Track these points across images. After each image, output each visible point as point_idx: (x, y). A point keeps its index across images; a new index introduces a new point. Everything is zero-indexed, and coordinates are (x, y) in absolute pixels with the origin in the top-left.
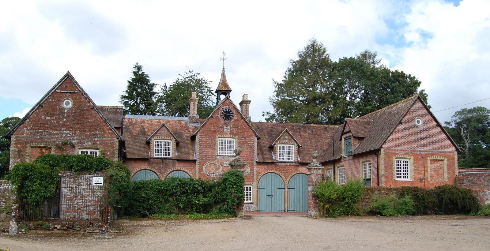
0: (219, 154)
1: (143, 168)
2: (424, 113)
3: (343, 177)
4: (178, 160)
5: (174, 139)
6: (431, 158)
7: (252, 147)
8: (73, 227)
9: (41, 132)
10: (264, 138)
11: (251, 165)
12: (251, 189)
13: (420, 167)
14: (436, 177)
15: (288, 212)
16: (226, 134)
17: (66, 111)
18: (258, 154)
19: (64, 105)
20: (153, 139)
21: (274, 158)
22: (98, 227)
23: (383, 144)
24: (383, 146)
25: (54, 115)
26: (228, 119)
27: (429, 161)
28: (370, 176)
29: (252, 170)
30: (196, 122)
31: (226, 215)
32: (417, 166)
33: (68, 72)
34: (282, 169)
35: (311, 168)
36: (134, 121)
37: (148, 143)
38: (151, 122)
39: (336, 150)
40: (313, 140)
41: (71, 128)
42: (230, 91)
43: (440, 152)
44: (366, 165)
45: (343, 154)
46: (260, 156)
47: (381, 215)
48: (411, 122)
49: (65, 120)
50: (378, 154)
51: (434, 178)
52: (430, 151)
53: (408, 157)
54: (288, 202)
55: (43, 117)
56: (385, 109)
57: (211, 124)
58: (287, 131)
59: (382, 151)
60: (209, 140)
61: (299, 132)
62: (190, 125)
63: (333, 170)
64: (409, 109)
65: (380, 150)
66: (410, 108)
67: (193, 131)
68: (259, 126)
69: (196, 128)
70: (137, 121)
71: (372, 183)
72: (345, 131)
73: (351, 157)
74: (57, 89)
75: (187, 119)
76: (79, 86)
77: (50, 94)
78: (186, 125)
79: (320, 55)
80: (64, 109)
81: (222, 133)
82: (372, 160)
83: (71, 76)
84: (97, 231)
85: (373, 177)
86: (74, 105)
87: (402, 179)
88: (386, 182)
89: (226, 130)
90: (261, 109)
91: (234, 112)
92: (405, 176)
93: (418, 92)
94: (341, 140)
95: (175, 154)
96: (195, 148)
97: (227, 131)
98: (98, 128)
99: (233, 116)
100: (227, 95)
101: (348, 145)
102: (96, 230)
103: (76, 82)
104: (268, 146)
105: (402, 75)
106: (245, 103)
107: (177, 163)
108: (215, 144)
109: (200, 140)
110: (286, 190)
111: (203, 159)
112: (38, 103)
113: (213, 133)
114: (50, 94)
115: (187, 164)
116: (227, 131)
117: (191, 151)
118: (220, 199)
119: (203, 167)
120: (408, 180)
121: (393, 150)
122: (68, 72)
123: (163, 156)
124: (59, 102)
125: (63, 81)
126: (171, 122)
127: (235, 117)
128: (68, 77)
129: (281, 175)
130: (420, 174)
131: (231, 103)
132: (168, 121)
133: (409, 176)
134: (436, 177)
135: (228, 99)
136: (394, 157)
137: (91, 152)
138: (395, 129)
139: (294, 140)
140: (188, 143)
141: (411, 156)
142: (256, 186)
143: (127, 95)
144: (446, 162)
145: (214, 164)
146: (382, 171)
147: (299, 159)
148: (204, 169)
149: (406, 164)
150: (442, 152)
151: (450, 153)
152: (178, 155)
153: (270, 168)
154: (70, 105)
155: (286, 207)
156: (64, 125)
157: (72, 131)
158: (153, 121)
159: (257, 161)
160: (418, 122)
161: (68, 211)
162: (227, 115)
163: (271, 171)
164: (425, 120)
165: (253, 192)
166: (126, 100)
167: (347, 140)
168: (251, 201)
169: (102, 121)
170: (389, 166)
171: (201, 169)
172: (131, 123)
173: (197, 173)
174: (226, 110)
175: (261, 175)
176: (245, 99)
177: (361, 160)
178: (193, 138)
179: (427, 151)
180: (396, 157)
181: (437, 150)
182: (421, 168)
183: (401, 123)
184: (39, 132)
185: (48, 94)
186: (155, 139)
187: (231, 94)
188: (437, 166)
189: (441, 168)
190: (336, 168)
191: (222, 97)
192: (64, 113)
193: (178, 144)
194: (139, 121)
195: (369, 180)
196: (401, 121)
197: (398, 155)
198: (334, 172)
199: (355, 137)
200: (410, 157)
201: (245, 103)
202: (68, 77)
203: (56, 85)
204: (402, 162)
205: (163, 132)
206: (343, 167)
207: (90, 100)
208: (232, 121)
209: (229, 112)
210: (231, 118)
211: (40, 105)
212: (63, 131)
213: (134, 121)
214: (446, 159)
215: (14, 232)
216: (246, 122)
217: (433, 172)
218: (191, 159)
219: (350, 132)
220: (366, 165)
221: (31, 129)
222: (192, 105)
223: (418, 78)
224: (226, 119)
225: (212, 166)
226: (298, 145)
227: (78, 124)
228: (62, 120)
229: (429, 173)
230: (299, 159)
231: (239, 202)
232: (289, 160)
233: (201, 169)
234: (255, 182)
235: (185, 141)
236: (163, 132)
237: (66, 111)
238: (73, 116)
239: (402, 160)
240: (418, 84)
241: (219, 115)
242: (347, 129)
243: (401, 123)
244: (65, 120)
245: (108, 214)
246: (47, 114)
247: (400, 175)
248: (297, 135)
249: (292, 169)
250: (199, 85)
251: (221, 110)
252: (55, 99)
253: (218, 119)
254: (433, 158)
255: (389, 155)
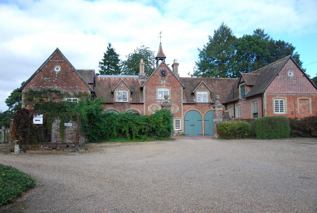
0: (158, 99)
1: (110, 109)
2: (294, 68)
3: (240, 112)
4: (132, 104)
5: (129, 90)
6: (300, 98)
7: (180, 94)
8: (56, 148)
9: (41, 87)
10: (189, 87)
11: (180, 105)
12: (180, 121)
13: (292, 104)
14: (303, 111)
15: (200, 135)
16: (163, 86)
17: (56, 73)
18: (184, 98)
19: (56, 70)
20: (115, 90)
21: (194, 101)
22: (72, 147)
23: (265, 90)
24: (265, 91)
25: (49, 76)
26: (164, 76)
27: (298, 100)
28: (257, 111)
29: (180, 108)
30: (144, 78)
31: (295, 136)
32: (289, 104)
33: (57, 48)
34: (200, 108)
35: (215, 107)
36: (104, 79)
37: (112, 93)
38: (115, 79)
39: (234, 93)
40: (221, 88)
41: (60, 84)
42: (165, 58)
43: (306, 94)
44: (254, 104)
45: (240, 97)
46: (185, 99)
47: (301, 136)
48: (285, 74)
49: (56, 79)
50: (262, 96)
51: (302, 111)
52: (299, 94)
53: (283, 98)
54: (204, 129)
55: (42, 78)
56: (268, 66)
57: (152, 80)
58: (203, 83)
59: (265, 94)
60: (152, 90)
61: (211, 83)
62: (140, 81)
63: (233, 107)
64: (284, 66)
65: (263, 94)
66: (284, 65)
67: (142, 85)
68: (184, 80)
69: (143, 82)
70: (105, 79)
71: (258, 116)
72: (241, 82)
73: (245, 99)
74: (51, 60)
75: (137, 76)
76: (65, 57)
77: (46, 63)
78: (137, 80)
79: (227, 32)
80: (55, 72)
81: (161, 85)
82: (258, 100)
83: (59, 51)
84: (71, 150)
85: (259, 112)
86: (62, 69)
87: (279, 113)
88: (268, 115)
89: (163, 83)
90: (187, 69)
91: (168, 71)
92: (281, 110)
93: (294, 54)
94: (238, 88)
95: (130, 99)
96: (143, 94)
97: (163, 84)
98: (77, 84)
99: (167, 74)
100: (163, 61)
101: (243, 91)
102: (70, 149)
103: (63, 55)
104: (190, 93)
105: (283, 43)
106: (175, 65)
107: (131, 105)
108: (155, 92)
109: (146, 90)
110: (203, 121)
111: (148, 103)
112: (39, 69)
113: (155, 85)
114: (46, 63)
115: (138, 106)
116: (163, 84)
117: (140, 97)
118: (157, 129)
119: (148, 107)
120: (284, 113)
121: (272, 93)
122: (57, 48)
123: (122, 101)
124: (52, 67)
125: (55, 53)
126: (128, 79)
127: (169, 74)
128: (57, 52)
129: (200, 112)
130: (292, 109)
131: (166, 66)
132: (125, 79)
133: (284, 110)
134: (303, 111)
135: (163, 63)
136: (273, 98)
137: (73, 100)
138: (274, 79)
139: (208, 88)
140: (138, 92)
141: (285, 97)
142: (183, 119)
143: (103, 62)
144: (310, 101)
145: (156, 106)
146: (265, 108)
147: (211, 101)
148: (149, 109)
149: (282, 102)
150: (307, 94)
151: (313, 95)
152: (132, 100)
153: (192, 107)
154: (59, 70)
155: (203, 132)
156: (55, 83)
157: (61, 86)
158: (116, 79)
159: (184, 103)
160: (290, 74)
161: (56, 138)
162: (163, 74)
163: (192, 109)
164: (295, 73)
165: (181, 122)
166: (103, 65)
167: (242, 88)
168: (180, 129)
169: (80, 80)
170: (270, 104)
171: (147, 109)
172: (102, 80)
173: (144, 111)
174: (162, 70)
175: (186, 112)
176: (175, 62)
177: (251, 101)
178: (142, 89)
179: (297, 94)
180: (275, 98)
181: (304, 93)
182: (292, 105)
183: (278, 75)
184: (40, 87)
185: (45, 63)
186: (117, 90)
187: (166, 60)
188: (304, 103)
189: (307, 105)
190: (236, 107)
191: (160, 62)
192: (56, 75)
193: (132, 93)
194: (107, 79)
195: (257, 113)
196: (278, 74)
197: (276, 97)
198: (234, 109)
199: (247, 86)
200: (284, 98)
201: (175, 65)
202: (57, 52)
203: (50, 57)
204: (279, 101)
205: (122, 86)
206: (240, 106)
207: (71, 66)
208: (167, 77)
209: (164, 71)
210: (166, 75)
211: (40, 70)
212: (55, 86)
213: (104, 79)
214: (311, 99)
215: (17, 152)
216: (176, 78)
217: (301, 108)
218: (141, 102)
219: (244, 82)
220: (254, 104)
221: (35, 85)
222: (141, 67)
223: (294, 45)
224: (162, 76)
225: (154, 107)
226: (210, 92)
227: (64, 82)
228: (54, 79)
229: (298, 108)
230: (211, 101)
231: (169, 129)
232: (205, 102)
233: (147, 109)
234: (183, 117)
235: (137, 91)
236: (122, 86)
237: (56, 73)
238: (61, 76)
239: (279, 100)
240: (293, 49)
241: (158, 73)
242: (242, 81)
243: (278, 75)
244: (56, 79)
245: (79, 139)
246: (45, 76)
247: (278, 110)
248: (210, 85)
249: (207, 107)
250: (148, 54)
251: (159, 71)
252: (49, 66)
253: (157, 76)
254: (301, 98)
255: (270, 97)
